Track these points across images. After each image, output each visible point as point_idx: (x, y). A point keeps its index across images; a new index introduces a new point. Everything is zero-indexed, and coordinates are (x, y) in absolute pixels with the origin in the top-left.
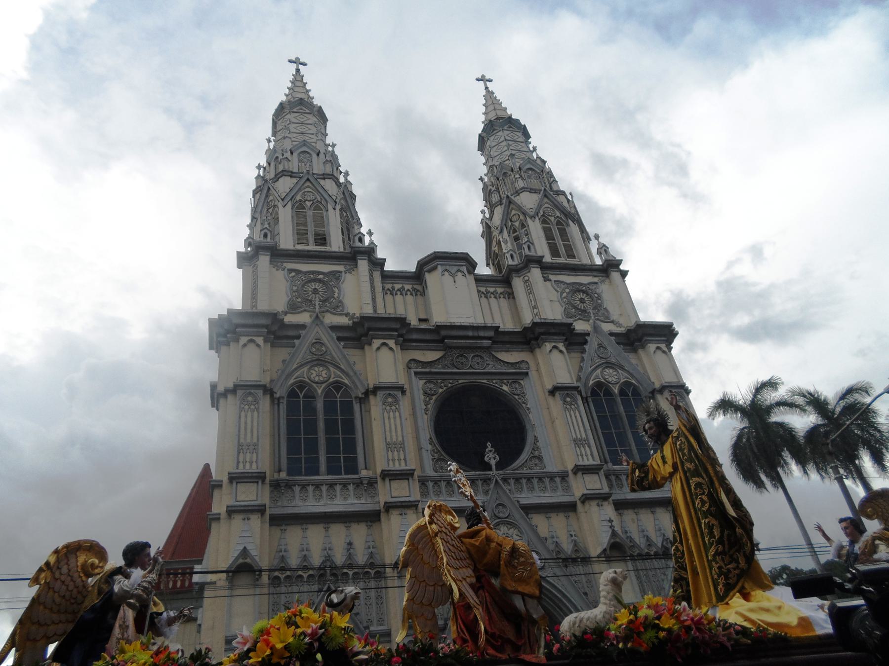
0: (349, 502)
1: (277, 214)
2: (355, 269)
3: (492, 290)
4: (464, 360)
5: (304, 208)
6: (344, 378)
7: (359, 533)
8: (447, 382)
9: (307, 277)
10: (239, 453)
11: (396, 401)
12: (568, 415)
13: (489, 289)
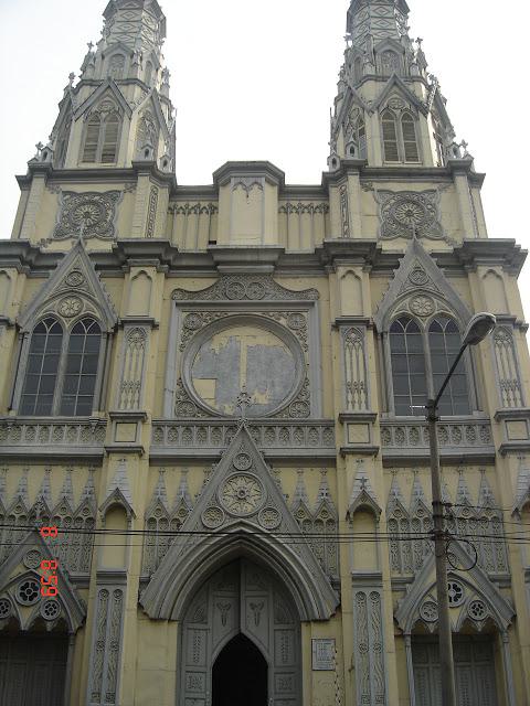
0: (74, 444)
3: (306, 203)
4: (239, 288)
7: (81, 476)
11: (143, 337)
12: (348, 355)
13: (292, 202)
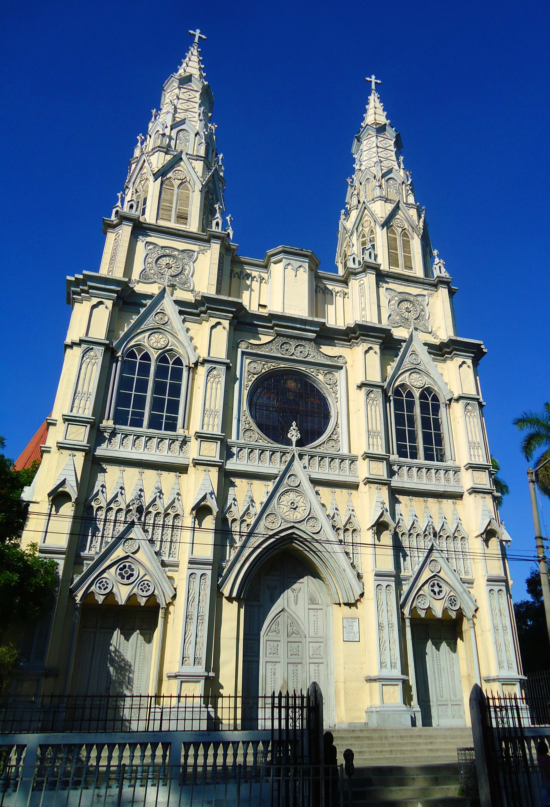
1: (148, 186)
6: (434, 385)
8: (269, 364)
9: (163, 252)
10: (369, 438)
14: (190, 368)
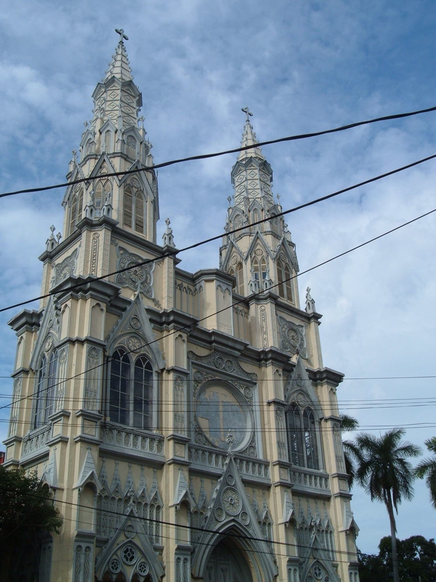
2: (162, 262)
5: (131, 193)
14: (158, 373)
